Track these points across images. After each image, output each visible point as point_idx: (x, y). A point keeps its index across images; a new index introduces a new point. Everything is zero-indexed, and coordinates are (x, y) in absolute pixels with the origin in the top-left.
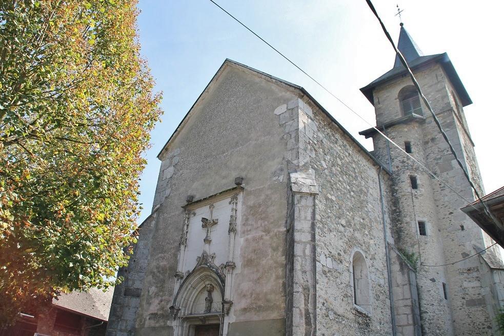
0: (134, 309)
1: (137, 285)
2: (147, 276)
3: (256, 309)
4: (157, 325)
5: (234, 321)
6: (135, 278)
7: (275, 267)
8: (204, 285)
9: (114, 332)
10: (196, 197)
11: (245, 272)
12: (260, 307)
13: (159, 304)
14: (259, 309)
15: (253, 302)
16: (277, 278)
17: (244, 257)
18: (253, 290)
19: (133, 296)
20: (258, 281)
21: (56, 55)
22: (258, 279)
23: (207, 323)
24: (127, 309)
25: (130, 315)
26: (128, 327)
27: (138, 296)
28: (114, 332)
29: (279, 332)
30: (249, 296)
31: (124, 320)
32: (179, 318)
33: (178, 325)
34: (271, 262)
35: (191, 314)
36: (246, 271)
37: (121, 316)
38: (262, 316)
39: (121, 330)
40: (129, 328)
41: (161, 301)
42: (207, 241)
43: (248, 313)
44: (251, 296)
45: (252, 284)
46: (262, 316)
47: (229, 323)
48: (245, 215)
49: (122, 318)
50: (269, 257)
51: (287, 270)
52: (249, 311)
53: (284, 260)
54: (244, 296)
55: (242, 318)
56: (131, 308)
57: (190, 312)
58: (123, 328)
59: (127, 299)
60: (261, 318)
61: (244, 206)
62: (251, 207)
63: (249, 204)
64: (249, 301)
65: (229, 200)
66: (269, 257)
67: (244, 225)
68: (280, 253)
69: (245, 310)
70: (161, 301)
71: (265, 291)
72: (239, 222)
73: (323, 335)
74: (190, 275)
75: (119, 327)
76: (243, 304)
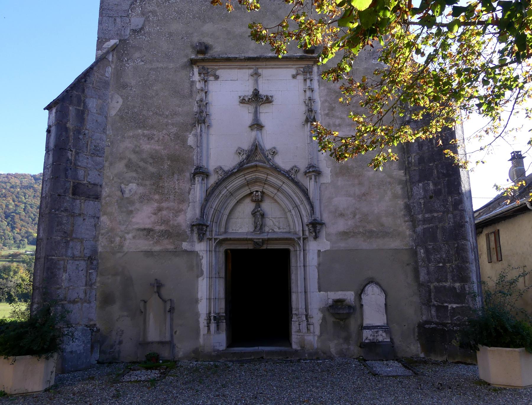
0: (92, 220)
4: (157, 248)
5: (328, 248)
6: (89, 166)
8: (248, 192)
10: (216, 50)
11: (339, 183)
12: (371, 232)
13: (155, 214)
14: (370, 235)
16: (395, 196)
18: (357, 209)
19: (88, 197)
22: (364, 195)
23: (264, 247)
31: (76, 238)
32: (210, 239)
36: (340, 182)
37: (72, 231)
39: (74, 258)
40: (87, 252)
41: (160, 209)
42: (257, 125)
44: (354, 216)
45: (354, 201)
47: (319, 251)
48: (326, 101)
49: (74, 236)
51: (474, 278)
52: (353, 236)
54: (342, 215)
55: (342, 245)
59: (78, 202)
60: (375, 246)
64: (350, 223)
65: (294, 72)
67: (327, 115)
69: (345, 235)
70: (160, 209)
71: (376, 212)
72: (318, 106)
73: (240, 2)
74: (229, 175)
75: (70, 253)
76: (341, 225)
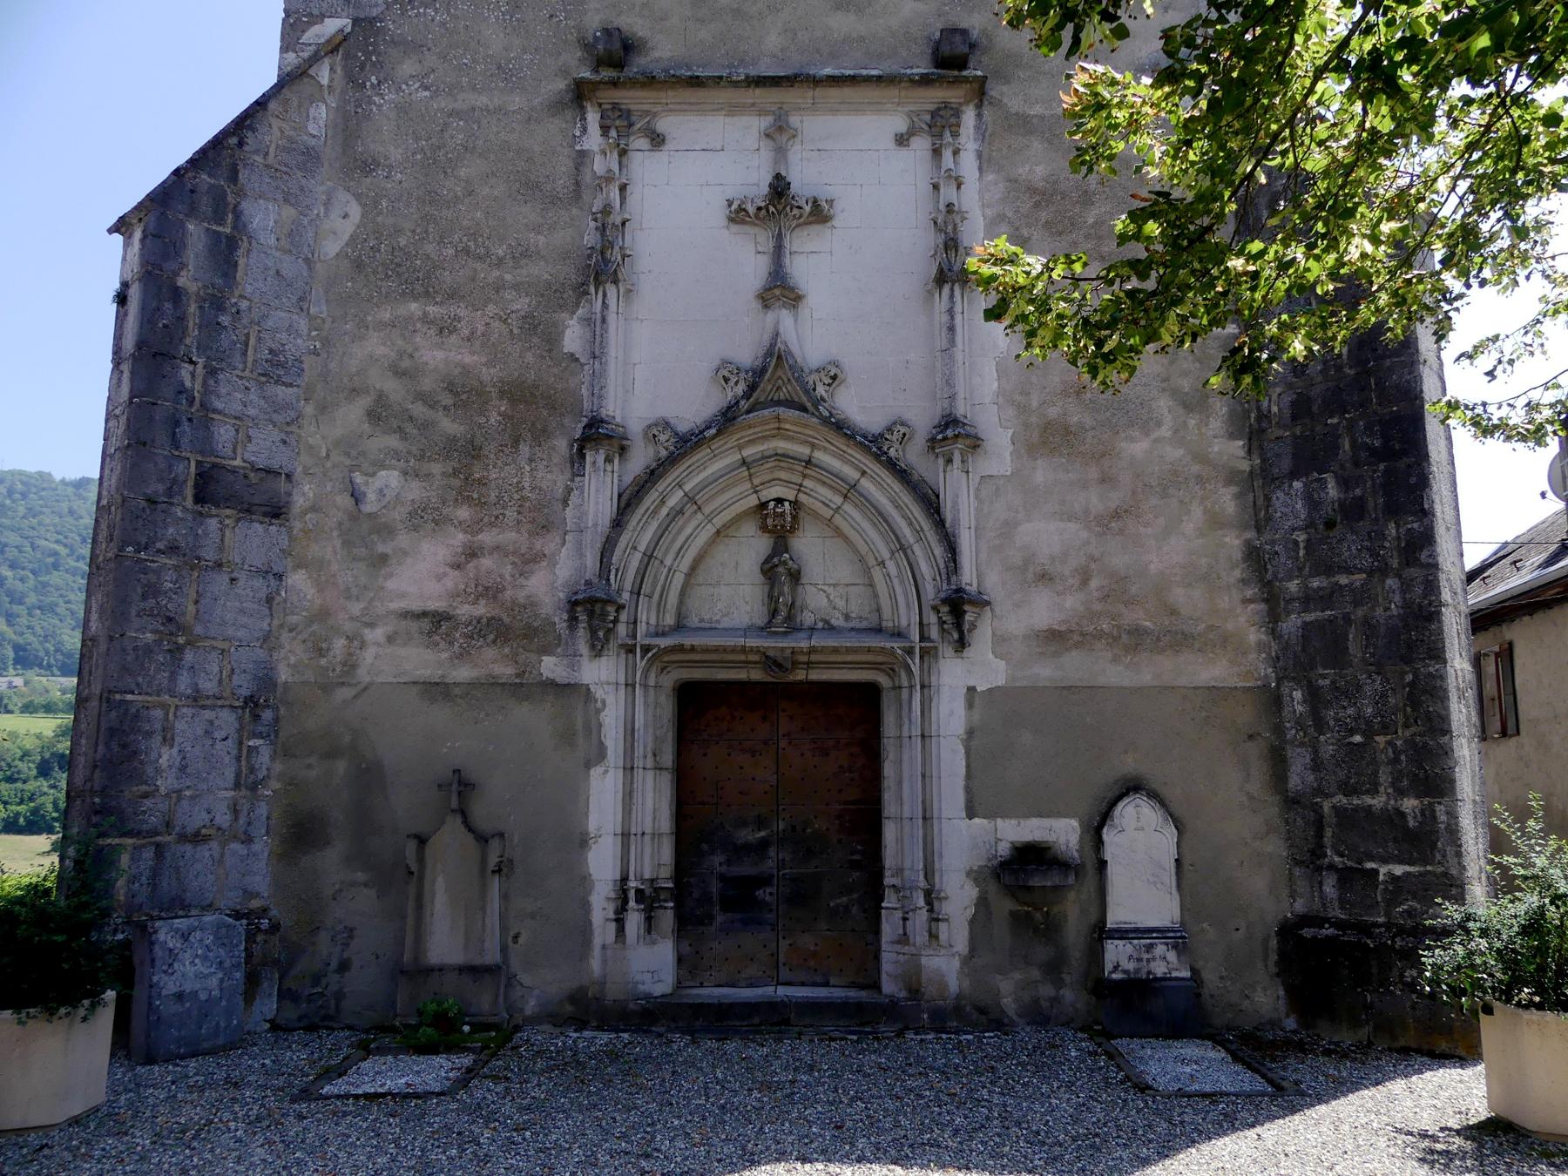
1: (262, 448)
2: (323, 408)
3: (1116, 639)
4: (463, 673)
6: (252, 412)
7: (1200, 479)
9: (158, 713)
12: (1137, 632)
14: (1134, 640)
15: (1098, 607)
16: (1215, 522)
17: (1022, 409)
19: (248, 510)
20: (1113, 520)
21: (1227, 194)
22: (1116, 515)
24: (222, 579)
25: (242, 611)
26: (236, 680)
27: (276, 512)
28: (158, 713)
29: (1251, 737)
30: (1075, 581)
33: (622, 680)
34: (1174, 453)
35: (679, 627)
36: (1042, 472)
38: (1147, 671)
41: (472, 553)
43: (1074, 653)
44: (1085, 582)
45: (1084, 534)
46: (1147, 671)
47: (971, 690)
50: (1165, 431)
52: (1077, 645)
53: (1242, 453)
54: (1044, 577)
55: (1045, 672)
56: (242, 577)
57: (669, 620)
58: (208, 686)
59: (213, 523)
60: (1146, 678)
61: (990, 177)
62: (1032, 190)
63: (1022, 171)
64: (1072, 602)
65: (900, 124)
66: (1165, 431)
68: (1217, 424)
69: (1054, 639)
70: (472, 553)
71: (1153, 568)
76: (1043, 610)
